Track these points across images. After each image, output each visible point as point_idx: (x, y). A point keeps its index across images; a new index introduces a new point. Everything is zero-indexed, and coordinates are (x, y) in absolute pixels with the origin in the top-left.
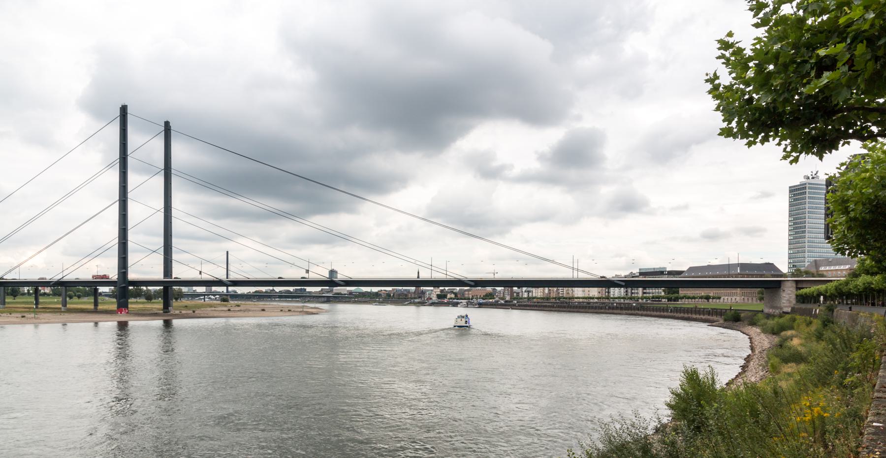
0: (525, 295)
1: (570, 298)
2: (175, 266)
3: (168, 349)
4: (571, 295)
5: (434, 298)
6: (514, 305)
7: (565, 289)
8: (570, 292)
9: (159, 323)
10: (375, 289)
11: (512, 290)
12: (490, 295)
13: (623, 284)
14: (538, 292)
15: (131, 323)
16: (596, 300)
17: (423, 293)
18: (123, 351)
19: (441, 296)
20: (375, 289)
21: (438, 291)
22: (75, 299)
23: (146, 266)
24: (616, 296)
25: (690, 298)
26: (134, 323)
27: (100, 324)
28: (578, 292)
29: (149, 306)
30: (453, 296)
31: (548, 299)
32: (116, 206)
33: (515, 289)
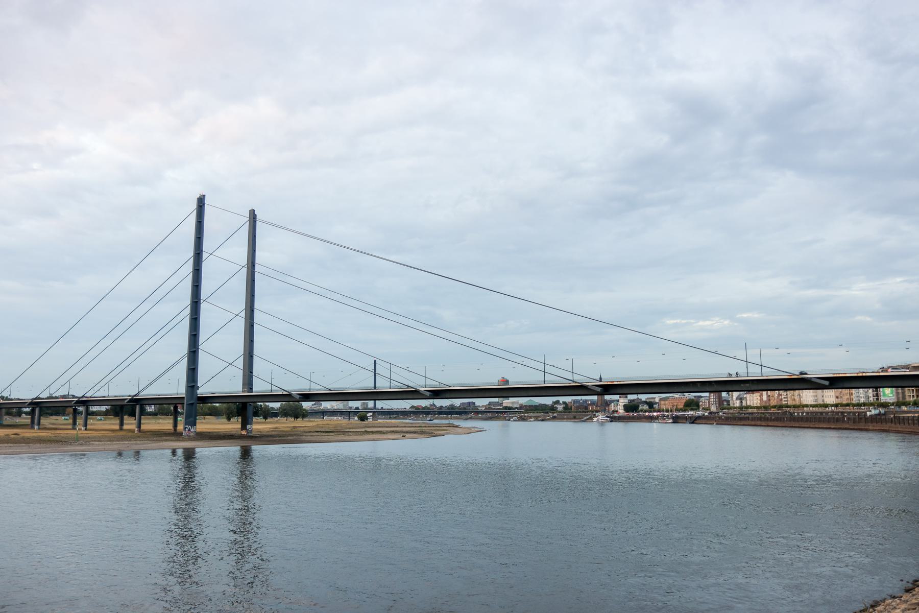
0: (737, 404)
1: (795, 406)
2: (256, 381)
3: (245, 477)
4: (797, 403)
5: (621, 411)
6: (720, 418)
7: (790, 393)
8: (797, 398)
9: (234, 450)
10: (548, 401)
11: (720, 397)
12: (692, 405)
13: (827, 383)
14: (753, 399)
15: (254, 447)
16: (755, 410)
17: (608, 403)
18: (188, 483)
19: (631, 407)
20: (548, 401)
21: (623, 401)
22: (260, 419)
23: (220, 377)
24: (862, 400)
25: (464, 431)
26: (204, 451)
27: (143, 453)
28: (808, 397)
29: (389, 421)
30: (646, 407)
31: (765, 408)
32: (203, 295)
33: (724, 394)
